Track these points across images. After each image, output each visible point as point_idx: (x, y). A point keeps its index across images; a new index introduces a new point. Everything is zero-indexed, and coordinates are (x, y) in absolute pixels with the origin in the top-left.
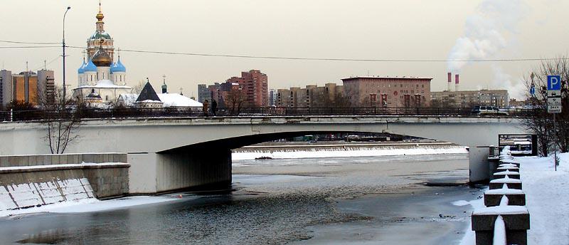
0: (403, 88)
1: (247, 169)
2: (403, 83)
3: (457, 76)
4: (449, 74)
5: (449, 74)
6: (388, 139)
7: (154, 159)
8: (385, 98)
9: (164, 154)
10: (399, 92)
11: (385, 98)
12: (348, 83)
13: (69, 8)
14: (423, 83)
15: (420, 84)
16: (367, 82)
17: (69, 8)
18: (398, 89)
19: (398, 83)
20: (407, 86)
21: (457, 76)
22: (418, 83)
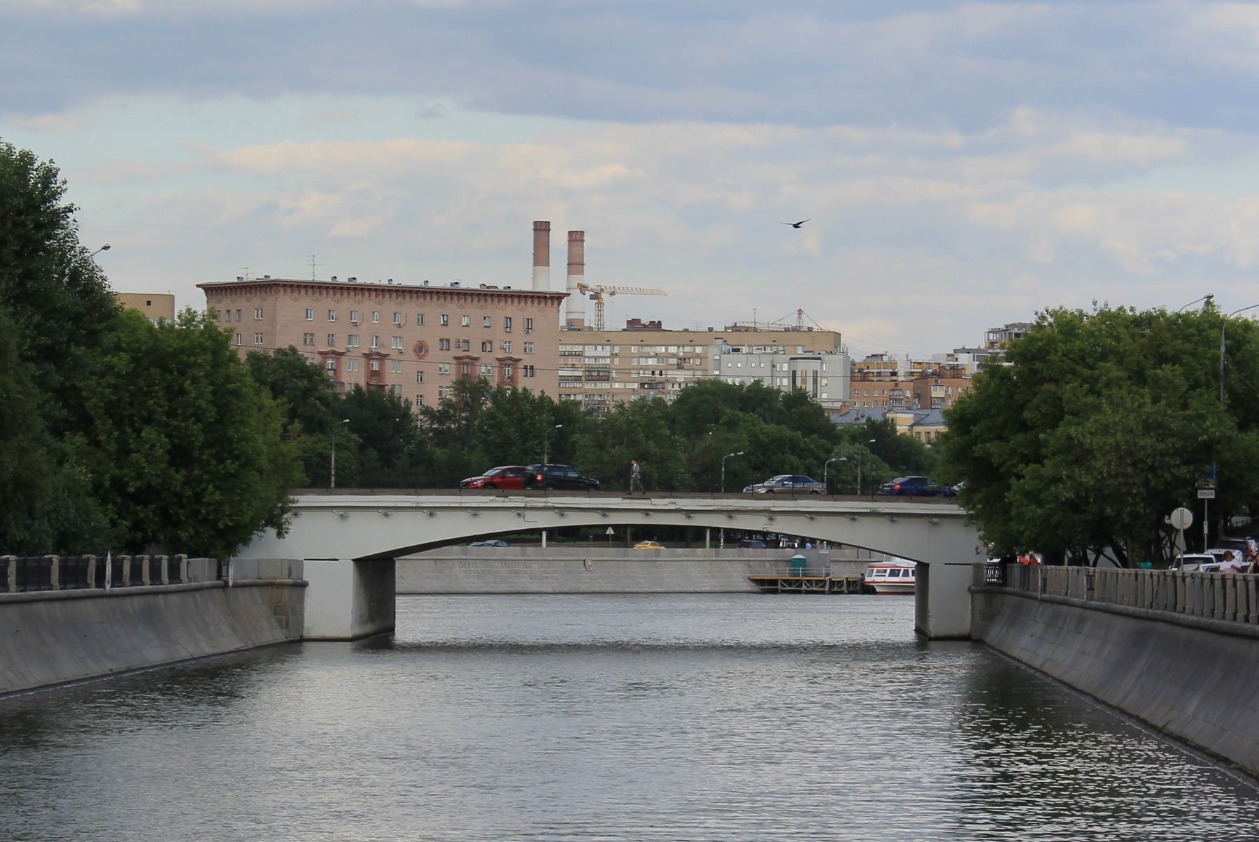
0: (453, 333)
1: (1212, 494)
2: (452, 307)
3: (576, 238)
4: (542, 228)
5: (542, 228)
6: (610, 531)
7: (350, 568)
8: (307, 358)
9: (353, 560)
10: (434, 346)
11: (307, 358)
12: (225, 304)
13: (106, 248)
14: (532, 310)
15: (517, 312)
16: (305, 301)
17: (106, 248)
18: (431, 334)
19: (433, 310)
20: (465, 318)
21: (576, 238)
22: (511, 309)
